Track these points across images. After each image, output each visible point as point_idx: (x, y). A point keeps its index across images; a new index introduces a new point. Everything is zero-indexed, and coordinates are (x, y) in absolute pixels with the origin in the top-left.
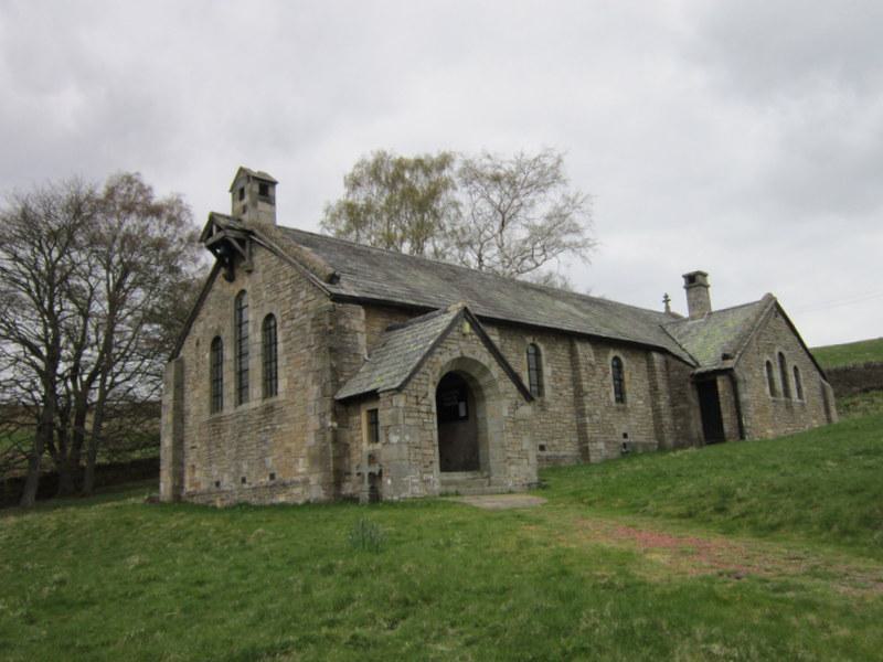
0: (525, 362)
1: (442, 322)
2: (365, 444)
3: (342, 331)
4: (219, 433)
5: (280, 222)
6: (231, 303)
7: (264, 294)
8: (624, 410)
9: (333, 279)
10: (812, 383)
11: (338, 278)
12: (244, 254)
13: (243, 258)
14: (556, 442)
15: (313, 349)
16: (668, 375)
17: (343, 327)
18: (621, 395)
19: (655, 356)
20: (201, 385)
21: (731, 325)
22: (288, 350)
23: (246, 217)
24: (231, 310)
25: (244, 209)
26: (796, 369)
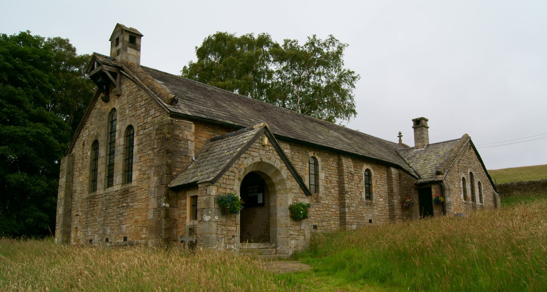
0: (307, 169)
1: (249, 135)
2: (188, 220)
3: (177, 139)
5: (143, 63)
6: (106, 117)
7: (127, 111)
8: (371, 204)
10: (488, 193)
11: (176, 101)
12: (115, 83)
13: (115, 86)
14: (324, 224)
15: (156, 151)
16: (400, 183)
17: (178, 136)
19: (393, 170)
21: (441, 153)
22: (140, 151)
23: (119, 58)
24: (105, 121)
25: (118, 52)
26: (479, 183)
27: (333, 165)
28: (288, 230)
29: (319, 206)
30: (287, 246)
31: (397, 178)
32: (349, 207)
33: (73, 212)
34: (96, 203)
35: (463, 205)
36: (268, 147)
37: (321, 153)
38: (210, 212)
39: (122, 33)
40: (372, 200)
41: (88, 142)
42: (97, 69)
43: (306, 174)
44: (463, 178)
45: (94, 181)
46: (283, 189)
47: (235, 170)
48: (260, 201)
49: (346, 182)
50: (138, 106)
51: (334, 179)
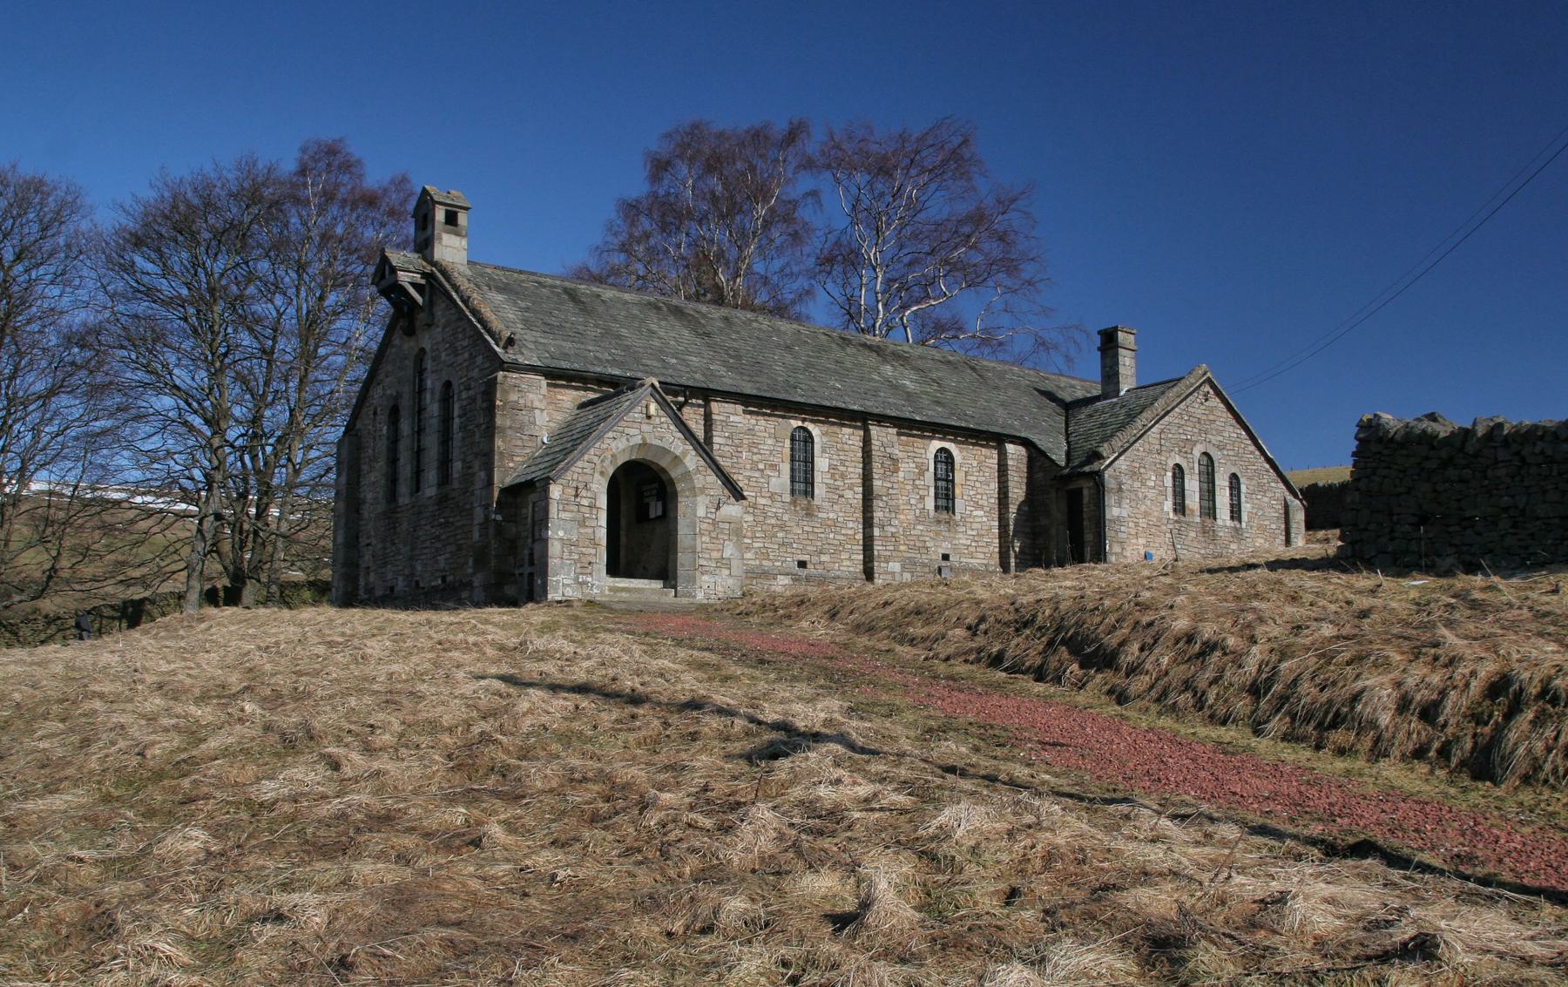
0: (787, 452)
4: (395, 528)
6: (409, 363)
7: (443, 354)
14: (824, 558)
18: (946, 498)
20: (377, 466)
22: (463, 428)
26: (1234, 479)
36: (657, 419)
45: (393, 480)
47: (595, 459)
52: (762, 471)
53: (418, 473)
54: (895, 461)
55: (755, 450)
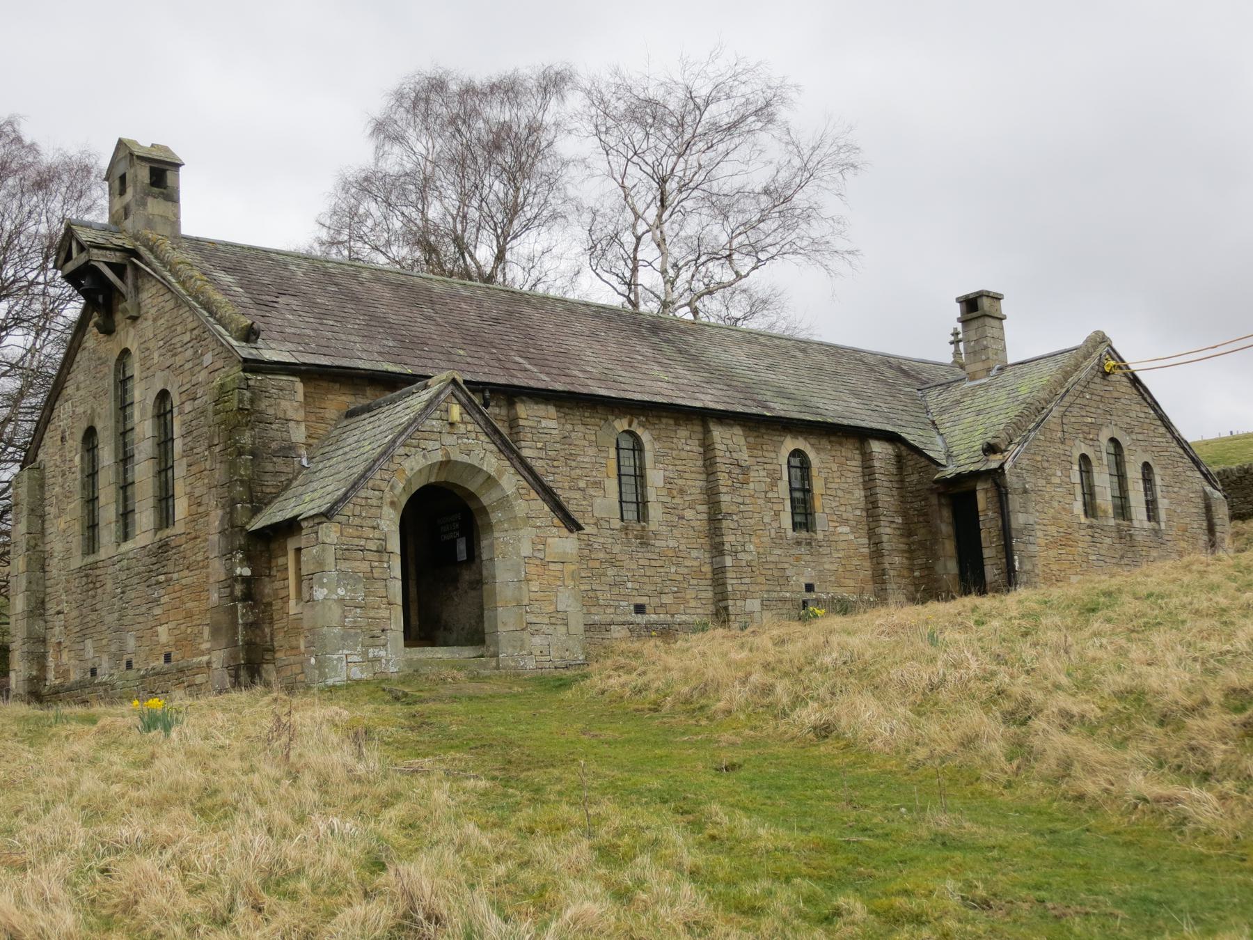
0: (613, 464)
6: (109, 370)
7: (156, 355)
9: (250, 335)
13: (123, 297)
14: (666, 599)
15: (217, 449)
16: (902, 481)
19: (877, 447)
22: (188, 452)
24: (109, 382)
27: (688, 448)
28: (522, 614)
29: (649, 555)
30: (521, 650)
31: (889, 467)
32: (736, 552)
33: (48, 606)
34: (100, 578)
35: (1083, 532)
36: (462, 427)
37: (651, 419)
38: (325, 580)
39: (132, 165)
40: (815, 532)
41: (72, 433)
42: (78, 259)
43: (608, 477)
44: (1084, 458)
45: (92, 527)
46: (509, 520)
47: (383, 485)
48: (462, 554)
49: (723, 490)
50: (179, 345)
51: (689, 483)
52: (583, 490)
53: (126, 516)
54: (745, 470)
55: (574, 464)
